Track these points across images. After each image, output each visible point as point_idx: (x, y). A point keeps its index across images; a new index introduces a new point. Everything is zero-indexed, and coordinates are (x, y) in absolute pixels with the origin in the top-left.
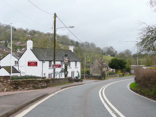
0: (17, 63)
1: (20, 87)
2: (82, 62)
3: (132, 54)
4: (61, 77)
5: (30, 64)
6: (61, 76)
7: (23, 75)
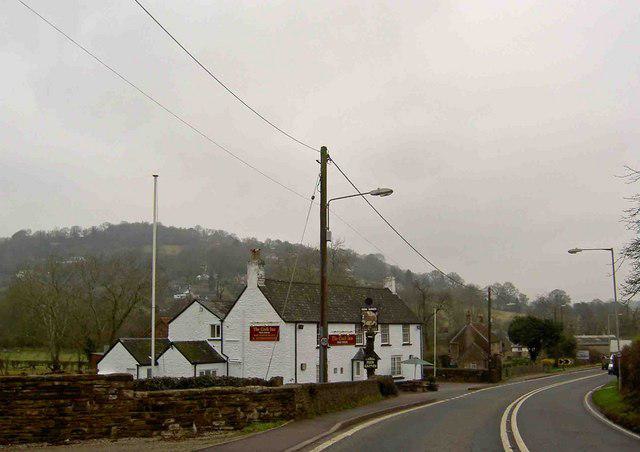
0: (217, 331)
1: (172, 421)
2: (424, 324)
3: (571, 304)
4: (357, 378)
5: (256, 334)
6: (358, 373)
7: (236, 373)
